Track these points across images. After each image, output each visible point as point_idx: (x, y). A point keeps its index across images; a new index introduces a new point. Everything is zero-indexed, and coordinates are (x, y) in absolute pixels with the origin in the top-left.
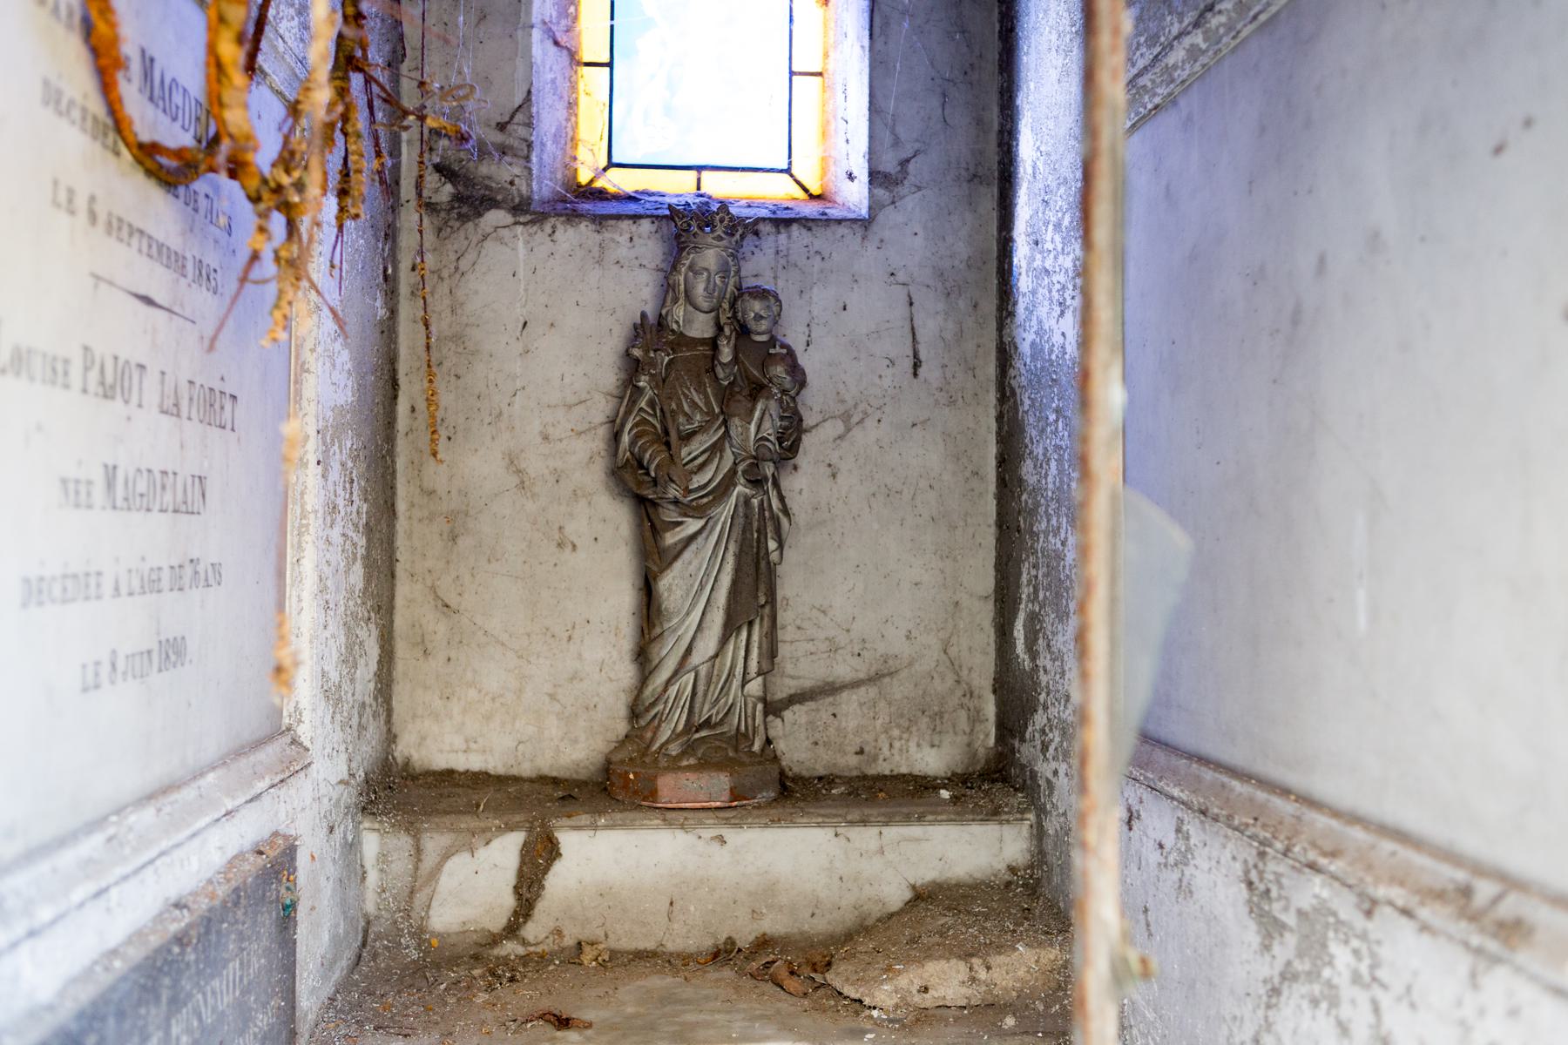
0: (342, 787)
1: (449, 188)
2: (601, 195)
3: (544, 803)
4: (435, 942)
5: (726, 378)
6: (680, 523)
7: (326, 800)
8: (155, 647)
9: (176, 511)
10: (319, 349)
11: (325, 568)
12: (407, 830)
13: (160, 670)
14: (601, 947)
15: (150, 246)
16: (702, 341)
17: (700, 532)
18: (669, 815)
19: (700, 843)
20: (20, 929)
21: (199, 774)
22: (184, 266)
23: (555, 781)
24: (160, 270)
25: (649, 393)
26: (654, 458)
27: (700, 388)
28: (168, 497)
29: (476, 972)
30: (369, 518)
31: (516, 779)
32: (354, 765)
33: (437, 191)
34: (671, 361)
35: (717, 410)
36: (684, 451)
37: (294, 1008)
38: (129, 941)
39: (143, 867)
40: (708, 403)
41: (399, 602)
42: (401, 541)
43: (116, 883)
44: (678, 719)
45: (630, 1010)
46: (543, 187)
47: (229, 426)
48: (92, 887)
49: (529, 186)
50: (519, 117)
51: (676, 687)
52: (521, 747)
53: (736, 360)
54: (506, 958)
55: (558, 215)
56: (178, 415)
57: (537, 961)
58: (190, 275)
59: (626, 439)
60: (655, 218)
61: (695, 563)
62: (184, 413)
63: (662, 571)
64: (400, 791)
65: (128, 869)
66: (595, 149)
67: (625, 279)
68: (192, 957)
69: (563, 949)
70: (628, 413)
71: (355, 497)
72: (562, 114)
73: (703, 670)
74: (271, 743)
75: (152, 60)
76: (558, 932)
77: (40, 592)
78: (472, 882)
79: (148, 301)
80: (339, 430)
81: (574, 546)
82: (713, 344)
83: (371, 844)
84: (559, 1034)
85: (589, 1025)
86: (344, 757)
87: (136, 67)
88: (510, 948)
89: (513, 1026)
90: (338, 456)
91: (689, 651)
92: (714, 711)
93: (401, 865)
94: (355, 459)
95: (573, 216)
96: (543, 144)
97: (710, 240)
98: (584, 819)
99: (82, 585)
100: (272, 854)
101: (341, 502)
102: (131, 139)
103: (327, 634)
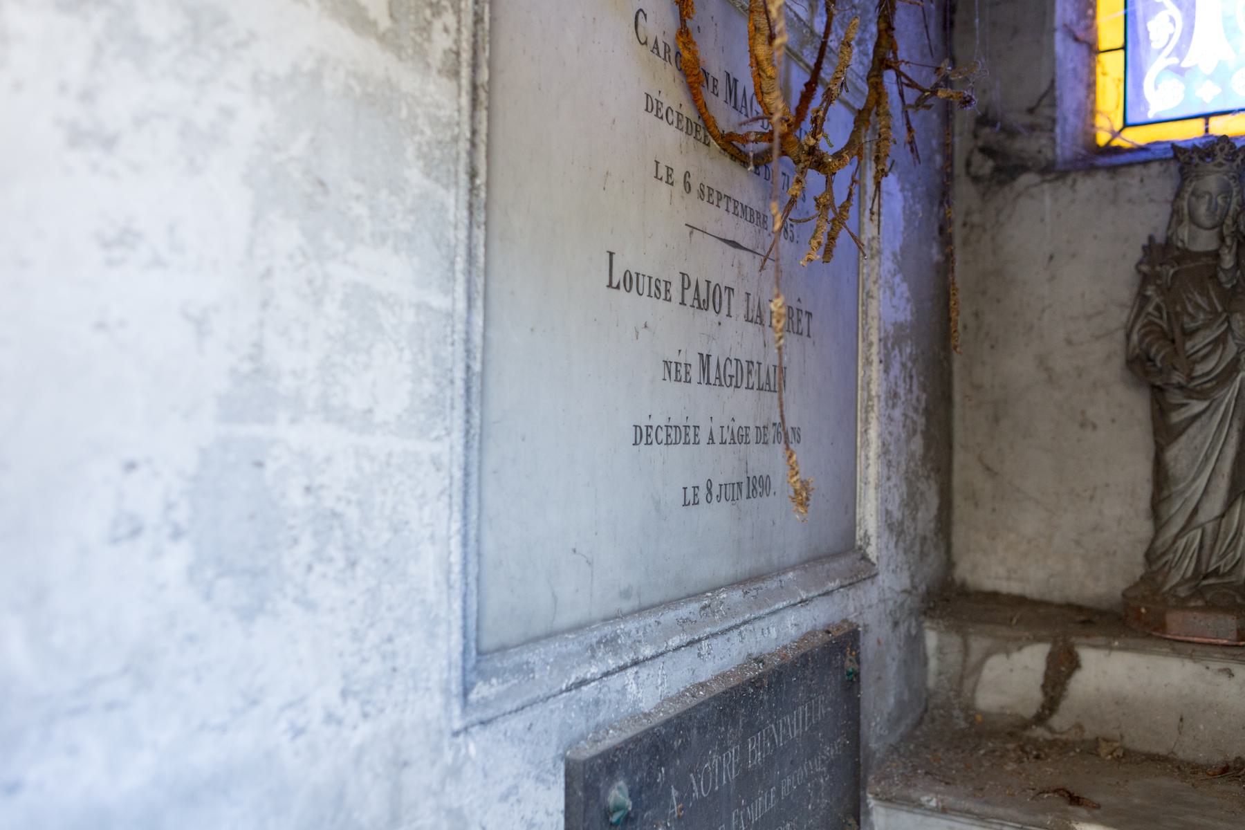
0: (905, 595)
1: (990, 164)
2: (1118, 150)
3: (1068, 624)
4: (979, 718)
5: (1230, 281)
7: (891, 603)
8: (745, 481)
10: (881, 282)
11: (888, 437)
12: (957, 632)
13: (748, 497)
14: (1116, 745)
15: (736, 207)
16: (1207, 254)
17: (1204, 411)
18: (1178, 646)
19: (1209, 674)
20: (627, 659)
21: (783, 570)
22: (765, 222)
23: (1080, 608)
24: (744, 224)
25: (1157, 300)
26: (1159, 352)
27: (1204, 293)
29: (1010, 746)
32: (917, 580)
34: (1176, 273)
35: (1220, 309)
36: (1189, 345)
37: (858, 747)
38: (716, 679)
39: (730, 629)
40: (1211, 303)
41: (956, 466)
42: (958, 426)
43: (707, 638)
44: (1188, 567)
45: (1136, 801)
46: (1065, 147)
47: (805, 333)
48: (686, 638)
49: (1054, 150)
50: (1045, 101)
51: (1184, 540)
53: (1237, 265)
54: (1036, 740)
56: (761, 323)
57: (1061, 747)
59: (1135, 337)
60: (1162, 161)
61: (1200, 438)
62: (767, 323)
64: (950, 600)
65: (717, 629)
66: (1112, 116)
67: (1144, 213)
68: (766, 698)
69: (1083, 741)
70: (1137, 316)
71: (915, 388)
72: (1081, 92)
73: (1210, 528)
74: (842, 557)
75: (736, 81)
76: (1080, 727)
77: (648, 435)
78: (1011, 677)
81: (1094, 427)
82: (1216, 255)
83: (931, 640)
84: (1070, 808)
85: (1098, 807)
87: (722, 86)
88: (1039, 732)
89: (1032, 793)
90: (898, 358)
91: (1195, 511)
92: (1222, 563)
93: (954, 657)
94: (914, 361)
96: (1065, 119)
97: (1211, 167)
98: (1100, 640)
99: (681, 434)
100: (838, 634)
101: (902, 392)
102: (716, 132)
103: (891, 484)
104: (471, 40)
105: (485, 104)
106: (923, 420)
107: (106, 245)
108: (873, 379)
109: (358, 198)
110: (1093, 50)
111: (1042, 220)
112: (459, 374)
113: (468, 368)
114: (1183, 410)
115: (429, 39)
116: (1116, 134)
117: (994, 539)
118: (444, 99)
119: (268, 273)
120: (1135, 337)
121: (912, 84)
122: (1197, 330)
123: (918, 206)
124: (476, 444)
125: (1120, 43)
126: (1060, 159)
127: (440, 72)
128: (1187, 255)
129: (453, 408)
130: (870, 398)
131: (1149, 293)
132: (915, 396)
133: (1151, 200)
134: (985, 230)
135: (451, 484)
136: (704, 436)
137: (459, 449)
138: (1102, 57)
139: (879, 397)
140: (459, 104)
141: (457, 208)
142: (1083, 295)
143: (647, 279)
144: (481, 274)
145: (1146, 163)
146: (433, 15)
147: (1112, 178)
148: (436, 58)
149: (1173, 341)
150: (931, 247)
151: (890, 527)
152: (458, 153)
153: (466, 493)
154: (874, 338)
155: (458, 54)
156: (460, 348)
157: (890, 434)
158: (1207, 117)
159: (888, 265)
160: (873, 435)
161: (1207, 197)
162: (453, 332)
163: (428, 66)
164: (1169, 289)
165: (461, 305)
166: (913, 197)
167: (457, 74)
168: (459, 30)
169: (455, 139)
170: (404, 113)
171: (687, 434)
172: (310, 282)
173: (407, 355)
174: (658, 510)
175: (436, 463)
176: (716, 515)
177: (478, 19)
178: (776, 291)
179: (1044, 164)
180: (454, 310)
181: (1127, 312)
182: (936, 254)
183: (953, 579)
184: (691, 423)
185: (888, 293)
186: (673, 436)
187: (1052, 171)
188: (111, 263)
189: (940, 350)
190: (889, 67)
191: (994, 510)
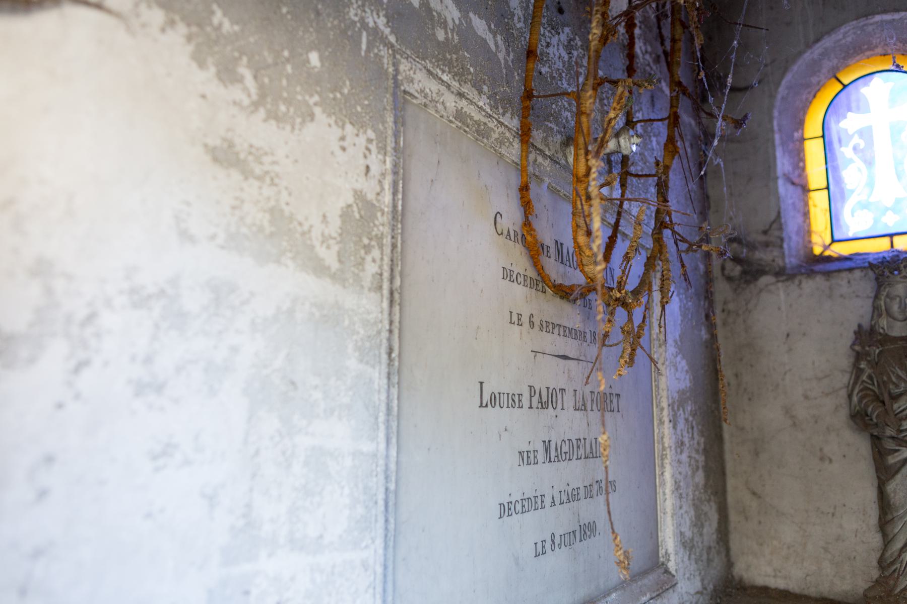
0: (698, 596)
1: (738, 269)
2: (829, 259)
6: (898, 450)
9: (585, 458)
10: (667, 363)
11: (678, 476)
13: (581, 541)
15: (565, 331)
21: (607, 593)
22: (585, 337)
25: (868, 371)
28: (581, 451)
30: (705, 446)
31: (807, 598)
32: (706, 582)
33: (732, 270)
36: (895, 406)
42: (728, 456)
47: (616, 409)
50: (775, 226)
52: (808, 578)
55: (802, 274)
56: (585, 410)
58: (589, 341)
59: (855, 399)
60: (862, 268)
62: (589, 408)
63: (888, 480)
66: (823, 235)
67: (853, 306)
70: (855, 383)
72: (800, 219)
75: (562, 244)
79: (565, 357)
80: (681, 403)
81: (831, 461)
86: (698, 578)
87: (553, 250)
90: (682, 416)
95: (811, 274)
96: (790, 238)
97: (898, 278)
99: (532, 503)
101: (686, 440)
103: (682, 511)
104: (390, 263)
105: (398, 301)
106: (703, 458)
107: (155, 458)
108: (666, 434)
109: (316, 387)
110: (805, 189)
111: (779, 309)
112: (381, 497)
113: (387, 489)
114: (896, 454)
115: (363, 270)
116: (826, 247)
117: (761, 545)
118: (370, 306)
119: (257, 453)
120: (855, 399)
121: (684, 240)
122: (901, 395)
123: (690, 304)
124: (391, 544)
125: (824, 185)
126: (788, 266)
127: (370, 290)
128: (887, 339)
129: (376, 521)
130: (664, 449)
131: (862, 366)
132: (696, 442)
133: (857, 296)
134: (738, 315)
135: (375, 579)
136: (548, 501)
137: (381, 551)
138: (812, 194)
139: (670, 447)
140: (382, 308)
141: (380, 378)
142: (813, 363)
143: (506, 395)
144: (395, 419)
145: (850, 270)
146: (366, 253)
147: (828, 280)
148: (367, 280)
149: (883, 402)
150: (701, 330)
151: (684, 545)
152: (381, 341)
153: (385, 582)
154: (665, 404)
155: (381, 275)
156: (381, 477)
157: (680, 473)
158: (891, 236)
159: (671, 349)
160: (668, 475)
161: (898, 299)
162: (377, 466)
163: (362, 287)
164: (877, 364)
165: (382, 446)
166: (686, 298)
167: (380, 288)
168: (382, 259)
169: (379, 332)
170: (347, 322)
171: (536, 503)
172: (284, 453)
173: (347, 491)
174: (517, 564)
175: (365, 566)
176: (557, 560)
177: (394, 246)
178: (602, 430)
179: (777, 269)
180: (377, 451)
181: (847, 376)
182: (704, 335)
183: (733, 576)
184: (538, 494)
185: (673, 370)
186: (526, 506)
187: (782, 274)
188: (157, 470)
189: (713, 405)
190: (666, 227)
191: (760, 522)
